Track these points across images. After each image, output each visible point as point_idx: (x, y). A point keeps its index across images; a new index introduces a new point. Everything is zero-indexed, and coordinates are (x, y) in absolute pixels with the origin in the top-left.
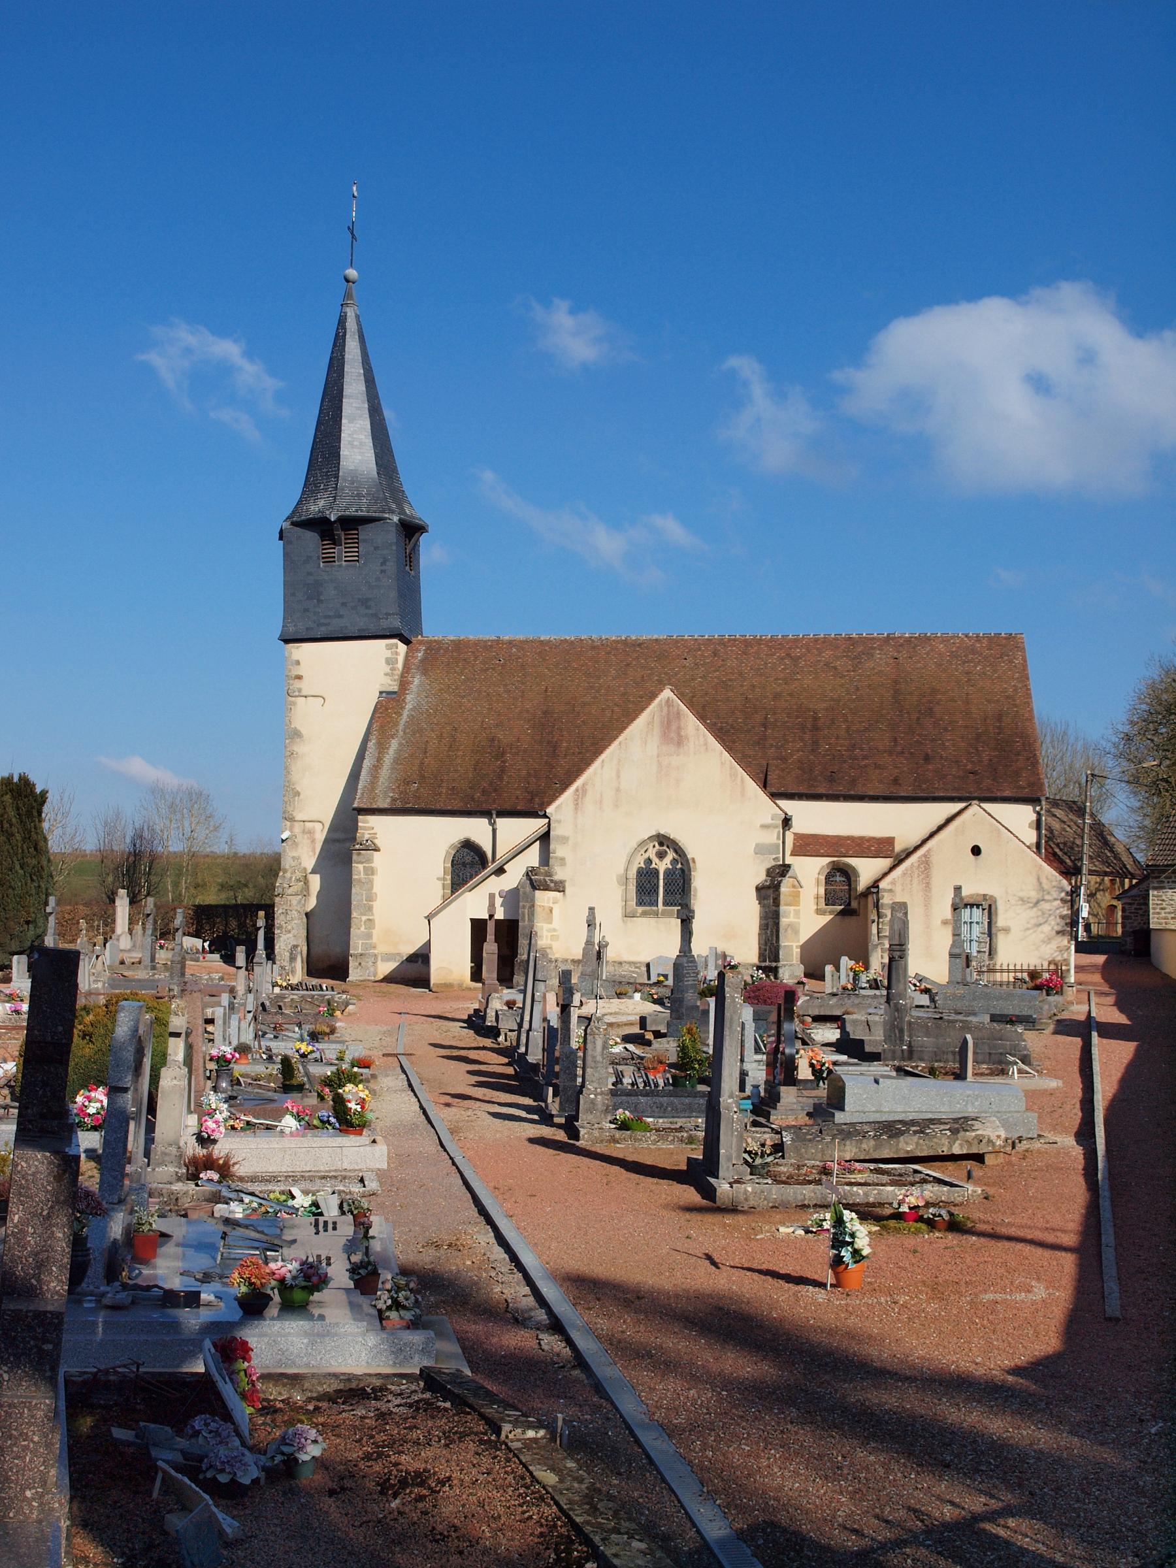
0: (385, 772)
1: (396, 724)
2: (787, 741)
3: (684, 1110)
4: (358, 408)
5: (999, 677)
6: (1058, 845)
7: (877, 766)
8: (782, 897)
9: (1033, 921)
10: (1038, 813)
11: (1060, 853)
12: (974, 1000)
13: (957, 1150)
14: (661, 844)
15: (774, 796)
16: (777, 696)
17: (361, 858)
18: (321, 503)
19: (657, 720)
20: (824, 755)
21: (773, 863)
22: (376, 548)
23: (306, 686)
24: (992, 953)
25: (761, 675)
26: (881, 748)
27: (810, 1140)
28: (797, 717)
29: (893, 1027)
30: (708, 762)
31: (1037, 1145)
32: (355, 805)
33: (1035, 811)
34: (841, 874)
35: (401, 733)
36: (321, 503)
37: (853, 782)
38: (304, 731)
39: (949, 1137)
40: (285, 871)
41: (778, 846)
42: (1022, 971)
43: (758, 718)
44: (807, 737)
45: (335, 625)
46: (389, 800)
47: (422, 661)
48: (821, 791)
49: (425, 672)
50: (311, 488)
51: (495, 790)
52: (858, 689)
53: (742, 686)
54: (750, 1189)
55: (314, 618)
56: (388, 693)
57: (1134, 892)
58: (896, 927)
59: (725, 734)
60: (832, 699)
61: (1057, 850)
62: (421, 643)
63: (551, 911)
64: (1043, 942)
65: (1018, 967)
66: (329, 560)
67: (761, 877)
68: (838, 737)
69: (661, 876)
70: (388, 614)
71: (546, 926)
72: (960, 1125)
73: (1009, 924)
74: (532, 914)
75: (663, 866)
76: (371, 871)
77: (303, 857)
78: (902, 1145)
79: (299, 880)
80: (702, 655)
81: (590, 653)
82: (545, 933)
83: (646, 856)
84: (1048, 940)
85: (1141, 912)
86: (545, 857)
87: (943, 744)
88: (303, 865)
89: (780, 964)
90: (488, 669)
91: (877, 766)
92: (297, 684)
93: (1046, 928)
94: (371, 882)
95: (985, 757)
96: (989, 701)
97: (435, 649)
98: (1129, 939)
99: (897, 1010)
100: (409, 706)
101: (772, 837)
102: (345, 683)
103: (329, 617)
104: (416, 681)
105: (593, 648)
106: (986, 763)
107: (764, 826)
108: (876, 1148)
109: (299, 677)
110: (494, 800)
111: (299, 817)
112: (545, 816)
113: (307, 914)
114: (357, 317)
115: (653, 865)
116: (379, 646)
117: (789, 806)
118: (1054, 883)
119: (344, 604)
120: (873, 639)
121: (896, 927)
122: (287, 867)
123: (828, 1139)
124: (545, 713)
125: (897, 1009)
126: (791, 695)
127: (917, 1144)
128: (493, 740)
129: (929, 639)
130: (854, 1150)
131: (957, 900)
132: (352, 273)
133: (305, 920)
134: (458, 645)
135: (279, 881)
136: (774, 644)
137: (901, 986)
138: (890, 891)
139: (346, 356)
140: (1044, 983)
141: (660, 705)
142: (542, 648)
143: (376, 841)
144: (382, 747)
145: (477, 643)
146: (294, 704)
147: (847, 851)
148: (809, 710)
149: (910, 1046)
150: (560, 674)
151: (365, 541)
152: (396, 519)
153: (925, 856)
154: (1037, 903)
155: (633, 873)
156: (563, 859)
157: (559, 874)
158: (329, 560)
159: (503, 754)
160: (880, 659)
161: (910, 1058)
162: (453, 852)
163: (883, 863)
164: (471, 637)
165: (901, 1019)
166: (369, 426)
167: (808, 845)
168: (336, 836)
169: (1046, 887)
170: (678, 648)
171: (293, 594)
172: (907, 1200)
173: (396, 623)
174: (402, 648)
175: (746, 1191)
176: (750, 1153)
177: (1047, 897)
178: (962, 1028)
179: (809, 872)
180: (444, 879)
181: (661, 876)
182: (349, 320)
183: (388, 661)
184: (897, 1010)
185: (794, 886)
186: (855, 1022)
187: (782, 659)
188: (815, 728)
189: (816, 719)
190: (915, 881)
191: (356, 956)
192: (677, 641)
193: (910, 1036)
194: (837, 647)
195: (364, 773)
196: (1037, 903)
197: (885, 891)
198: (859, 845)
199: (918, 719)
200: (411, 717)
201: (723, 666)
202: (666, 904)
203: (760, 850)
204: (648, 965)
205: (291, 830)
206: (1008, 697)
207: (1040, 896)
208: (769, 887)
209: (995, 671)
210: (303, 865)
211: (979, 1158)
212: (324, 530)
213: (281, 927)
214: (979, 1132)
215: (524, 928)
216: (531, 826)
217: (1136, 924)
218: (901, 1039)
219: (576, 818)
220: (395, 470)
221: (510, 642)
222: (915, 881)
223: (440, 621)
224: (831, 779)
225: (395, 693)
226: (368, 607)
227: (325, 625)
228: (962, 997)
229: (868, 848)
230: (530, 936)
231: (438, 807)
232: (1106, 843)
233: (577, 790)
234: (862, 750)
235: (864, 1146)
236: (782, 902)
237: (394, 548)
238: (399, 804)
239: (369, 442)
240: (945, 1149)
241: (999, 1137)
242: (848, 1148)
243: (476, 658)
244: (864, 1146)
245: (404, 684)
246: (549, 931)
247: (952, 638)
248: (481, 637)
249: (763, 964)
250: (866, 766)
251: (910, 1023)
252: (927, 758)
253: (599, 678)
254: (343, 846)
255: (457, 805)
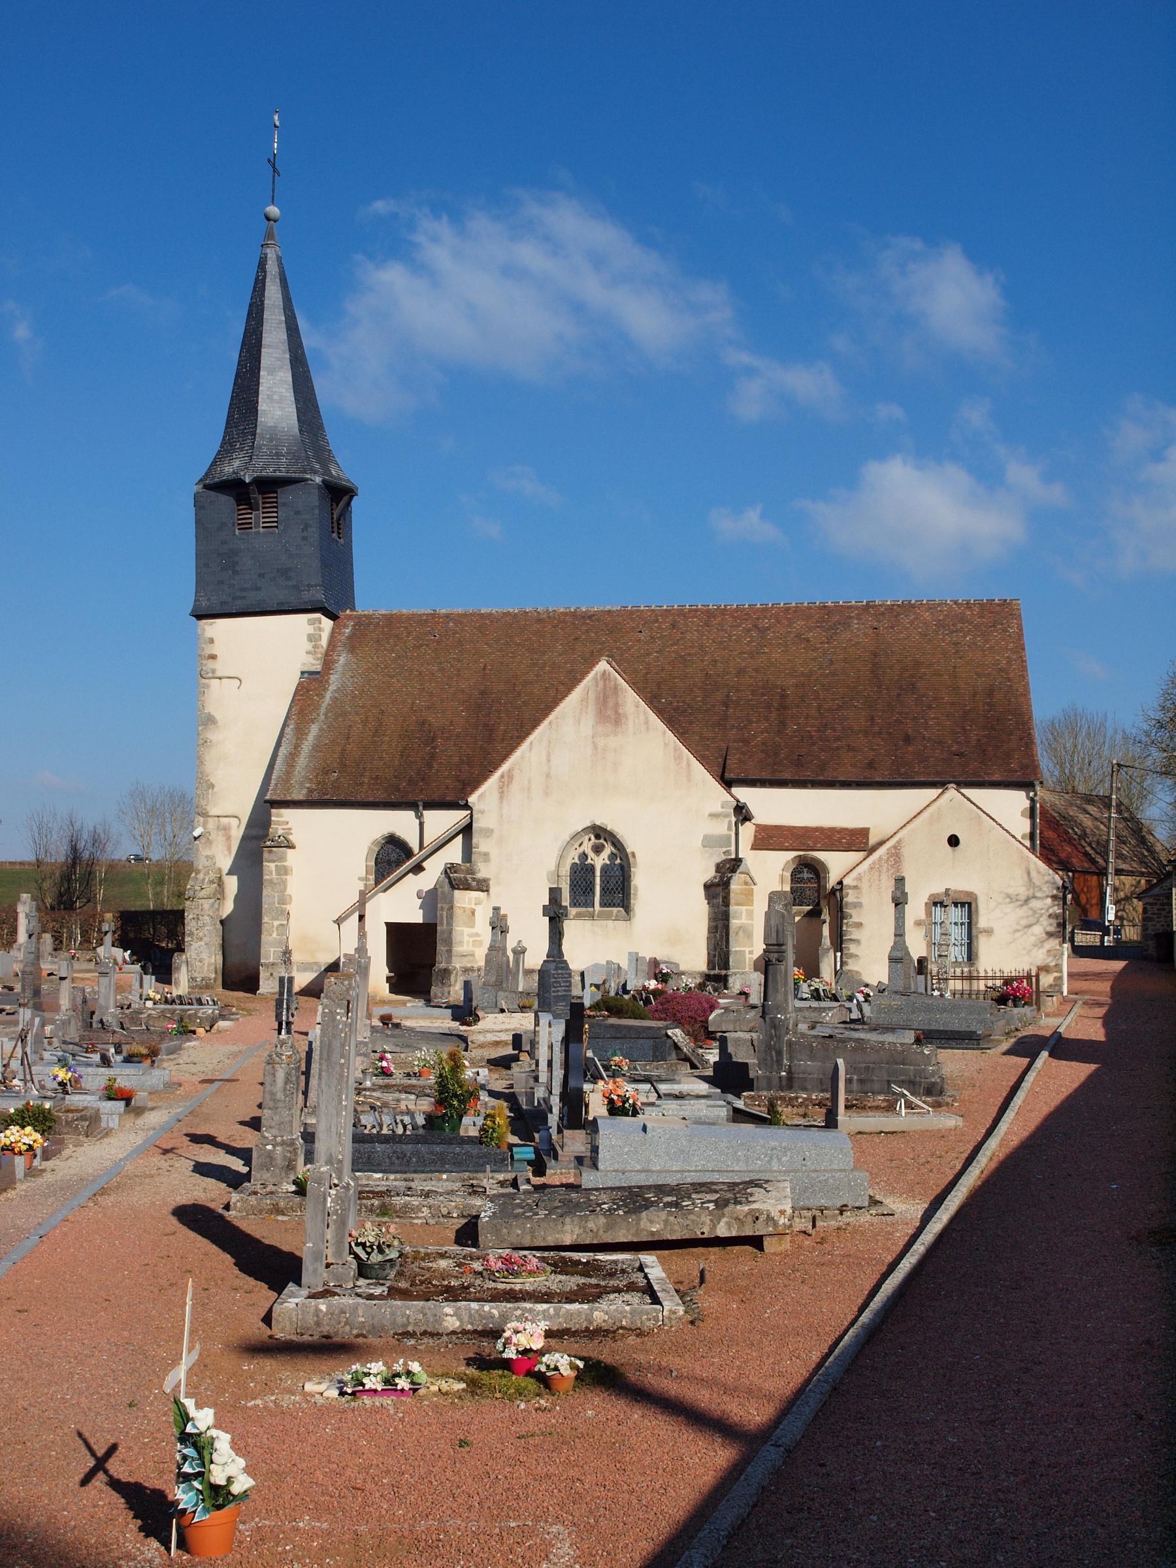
0: (302, 761)
1: (317, 707)
2: (750, 722)
3: (434, 1162)
4: (279, 359)
5: (991, 648)
6: (1090, 845)
7: (850, 748)
8: (732, 895)
9: (1024, 922)
10: (1032, 800)
11: (1091, 852)
12: (913, 1013)
13: (722, 1231)
14: (598, 837)
15: (728, 784)
16: (741, 672)
17: (272, 856)
18: (237, 463)
19: (592, 696)
20: (792, 737)
21: (724, 857)
22: (297, 513)
23: (220, 667)
24: (971, 956)
25: (724, 649)
26: (856, 728)
27: (517, 1216)
28: (763, 695)
29: (769, 1048)
30: (649, 741)
31: (865, 1218)
32: (267, 797)
33: (1028, 797)
34: (807, 873)
35: (322, 717)
36: (237, 463)
37: (823, 767)
38: (217, 715)
39: (711, 1213)
40: (198, 872)
41: (729, 837)
42: (994, 978)
43: (719, 696)
44: (773, 716)
45: (252, 598)
46: (304, 791)
47: (349, 638)
48: (786, 776)
49: (352, 650)
50: (227, 448)
51: (423, 780)
52: (832, 662)
53: (702, 661)
54: (323, 1308)
55: (229, 593)
56: (311, 673)
57: (1157, 891)
58: (773, 923)
59: (676, 717)
60: (803, 674)
61: (1088, 849)
62: (350, 618)
63: (473, 913)
64: (1035, 946)
65: (990, 974)
66: (245, 526)
67: (709, 874)
68: (807, 718)
69: (598, 873)
70: (308, 586)
71: (467, 931)
72: (736, 1192)
73: (991, 924)
74: (450, 917)
75: (599, 861)
76: (284, 871)
77: (219, 855)
78: (644, 1223)
79: (212, 882)
80: (659, 628)
81: (536, 627)
82: (466, 938)
83: (581, 850)
84: (1040, 943)
85: (1164, 913)
86: (468, 852)
87: (926, 722)
88: (217, 865)
89: (729, 972)
90: (421, 646)
91: (850, 748)
92: (210, 664)
93: (1038, 930)
94: (284, 883)
95: (973, 738)
96: (979, 675)
97: (364, 624)
98: (1151, 943)
99: (774, 1027)
100: (332, 688)
101: (722, 828)
102: (264, 662)
103: (243, 590)
104: (342, 660)
105: (539, 621)
106: (974, 743)
107: (713, 816)
108: (609, 1227)
109: (213, 657)
110: (422, 790)
111: (214, 811)
112: (467, 807)
113: (222, 922)
114: (279, 259)
115: (589, 861)
116: (300, 623)
117: (744, 794)
118: (1046, 878)
119: (261, 575)
120: (851, 607)
121: (773, 923)
122: (200, 867)
123: (542, 1213)
124: (483, 693)
125: (775, 1025)
126: (757, 670)
127: (666, 1221)
128: (423, 723)
129: (913, 606)
130: (577, 1231)
131: (898, 894)
132: (273, 210)
133: (219, 927)
134: (390, 620)
135: (191, 882)
136: (740, 615)
137: (780, 997)
138: (856, 887)
139: (266, 302)
140: (1013, 993)
141: (595, 678)
142: (483, 622)
143: (290, 837)
144: (300, 733)
145: (411, 618)
146: (208, 686)
147: (815, 844)
148: (776, 687)
149: (790, 1072)
150: (500, 650)
151: (284, 504)
152: (318, 480)
153: (895, 847)
154: (1027, 901)
155: (566, 870)
156: (486, 855)
157: (483, 871)
158: (245, 526)
159: (434, 739)
160: (858, 629)
161: (790, 1087)
162: (377, 849)
163: (853, 857)
164: (404, 611)
165: (779, 1038)
166: (290, 379)
167: (771, 837)
168: (254, 832)
169: (1038, 883)
170: (633, 619)
171: (206, 565)
172: (514, 1340)
173: (319, 595)
174: (327, 624)
175: (317, 1310)
176: (363, 1245)
177: (1038, 894)
178: (854, 1049)
179: (769, 872)
180: (366, 879)
181: (598, 873)
182: (269, 262)
183: (310, 638)
184: (774, 1027)
185: (746, 883)
186: (738, 1040)
187: (749, 630)
188: (783, 707)
189: (783, 696)
190: (884, 877)
191: (267, 965)
192: (631, 613)
193: (791, 1059)
194: (810, 617)
195: (279, 761)
196: (1027, 901)
197: (850, 887)
198: (829, 837)
199: (899, 695)
200: (334, 700)
201: (682, 638)
202: (603, 905)
203: (709, 842)
204: (582, 974)
205: (204, 826)
206: (1001, 670)
207: (1030, 893)
208: (718, 885)
209: (987, 641)
210: (217, 865)
211: (756, 1242)
212: (238, 493)
213: (191, 934)
214: (754, 1206)
215: (443, 932)
216: (456, 817)
217: (1158, 926)
218: (779, 1062)
219: (501, 808)
220: (321, 427)
221: (447, 616)
222: (884, 877)
223: (373, 594)
224: (799, 763)
225: (318, 673)
226: (289, 578)
227: (241, 598)
228: (899, 1010)
229: (839, 841)
230: (449, 942)
231: (359, 798)
232: (1143, 841)
233: (502, 776)
234: (834, 731)
235: (591, 1225)
236: (732, 901)
237: (317, 512)
238: (315, 796)
239: (290, 396)
240: (706, 1230)
241: (782, 1212)
242: (568, 1227)
243: (409, 634)
244: (591, 1225)
245: (328, 662)
246: (470, 936)
247: (939, 605)
248: (415, 610)
249: (712, 972)
250: (838, 748)
251: (790, 1041)
252: (907, 739)
253: (544, 653)
254: (258, 843)
255: (381, 796)
